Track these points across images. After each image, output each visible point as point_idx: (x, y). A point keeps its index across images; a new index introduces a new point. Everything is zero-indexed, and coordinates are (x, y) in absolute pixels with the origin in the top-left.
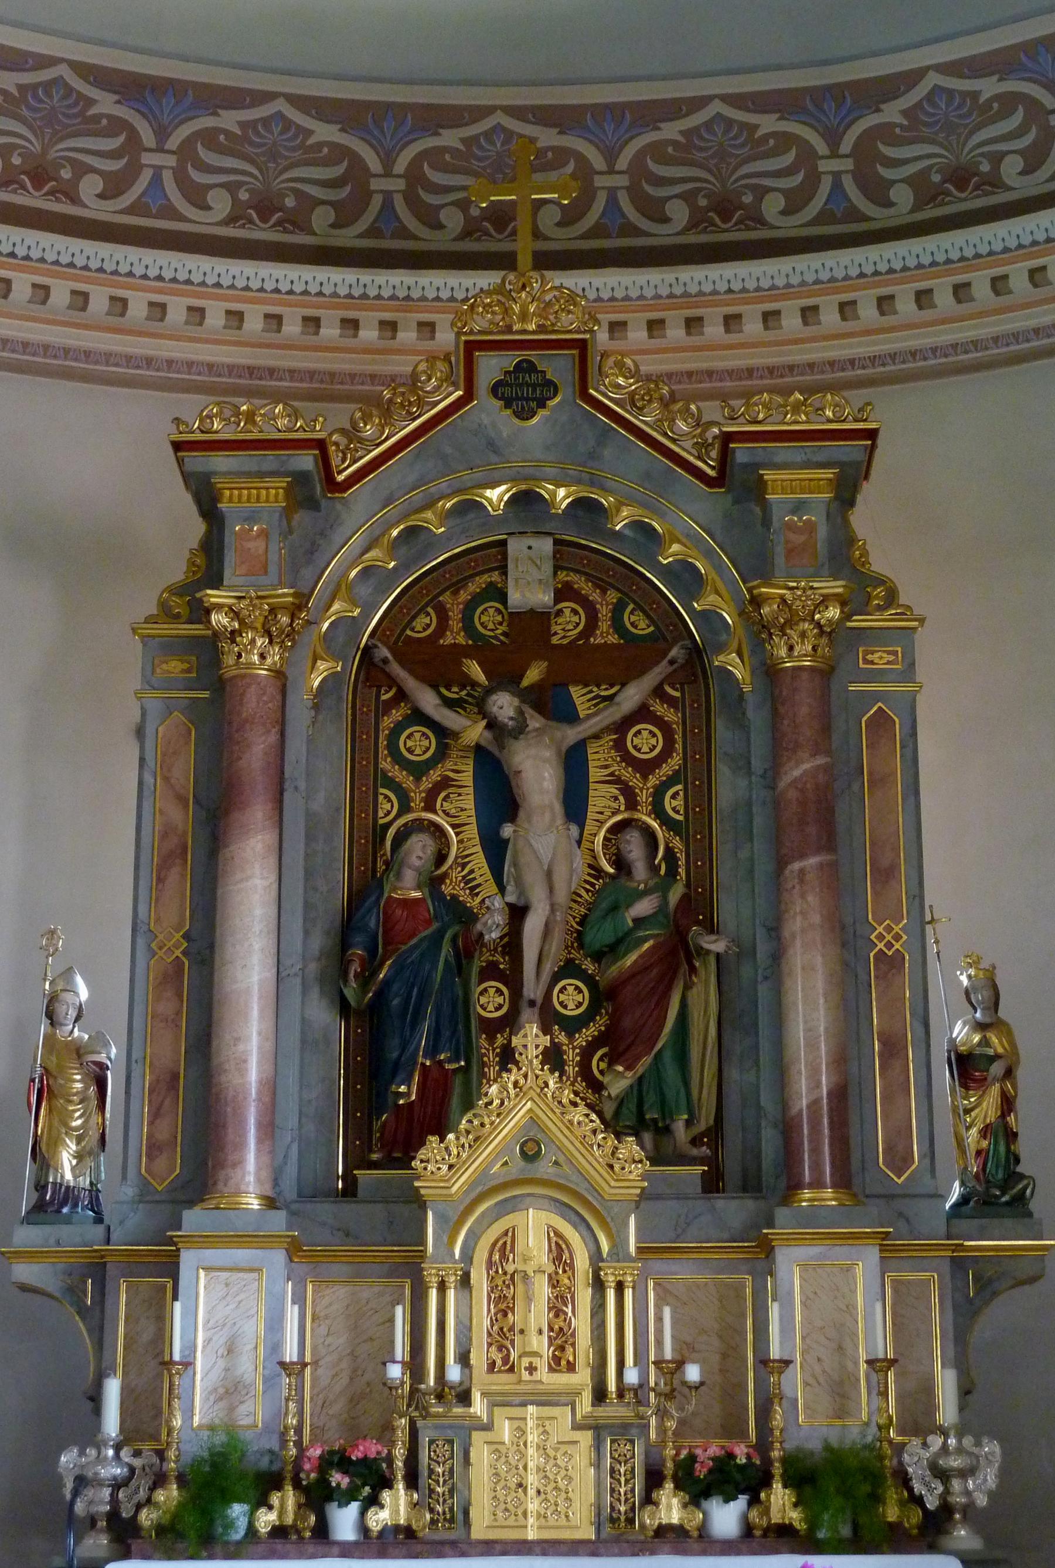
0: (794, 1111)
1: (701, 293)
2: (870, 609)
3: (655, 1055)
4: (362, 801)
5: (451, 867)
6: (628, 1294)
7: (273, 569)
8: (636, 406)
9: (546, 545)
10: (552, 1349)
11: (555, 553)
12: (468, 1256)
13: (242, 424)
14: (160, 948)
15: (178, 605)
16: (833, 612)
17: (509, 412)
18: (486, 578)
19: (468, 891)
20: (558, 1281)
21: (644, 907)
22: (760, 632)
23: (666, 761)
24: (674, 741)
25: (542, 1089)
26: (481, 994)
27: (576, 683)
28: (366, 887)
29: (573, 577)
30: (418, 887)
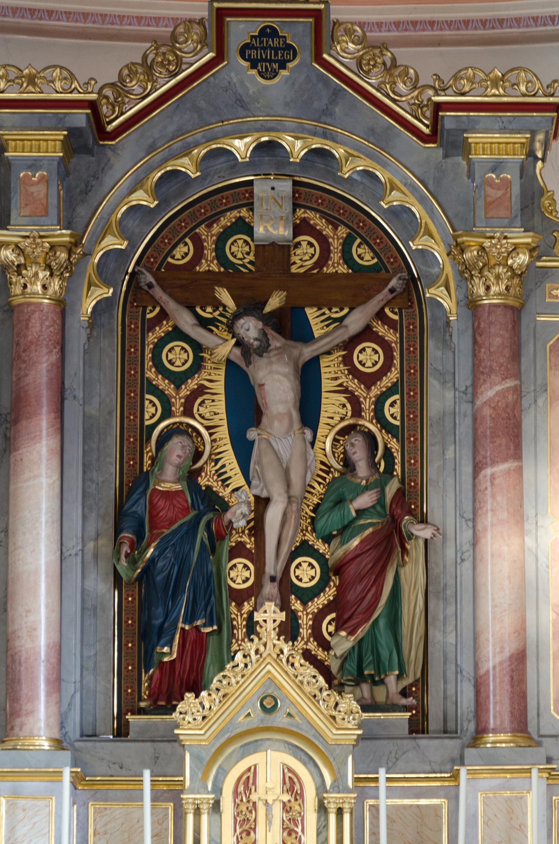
4: (130, 407)
5: (206, 463)
6: (347, 818)
7: (53, 212)
8: (362, 70)
11: (294, 192)
12: (218, 790)
17: (254, 72)
19: (220, 483)
20: (291, 808)
21: (365, 500)
23: (386, 375)
24: (392, 358)
25: (278, 655)
26: (231, 568)
27: (311, 306)
28: (134, 483)
29: (310, 214)
30: (178, 481)
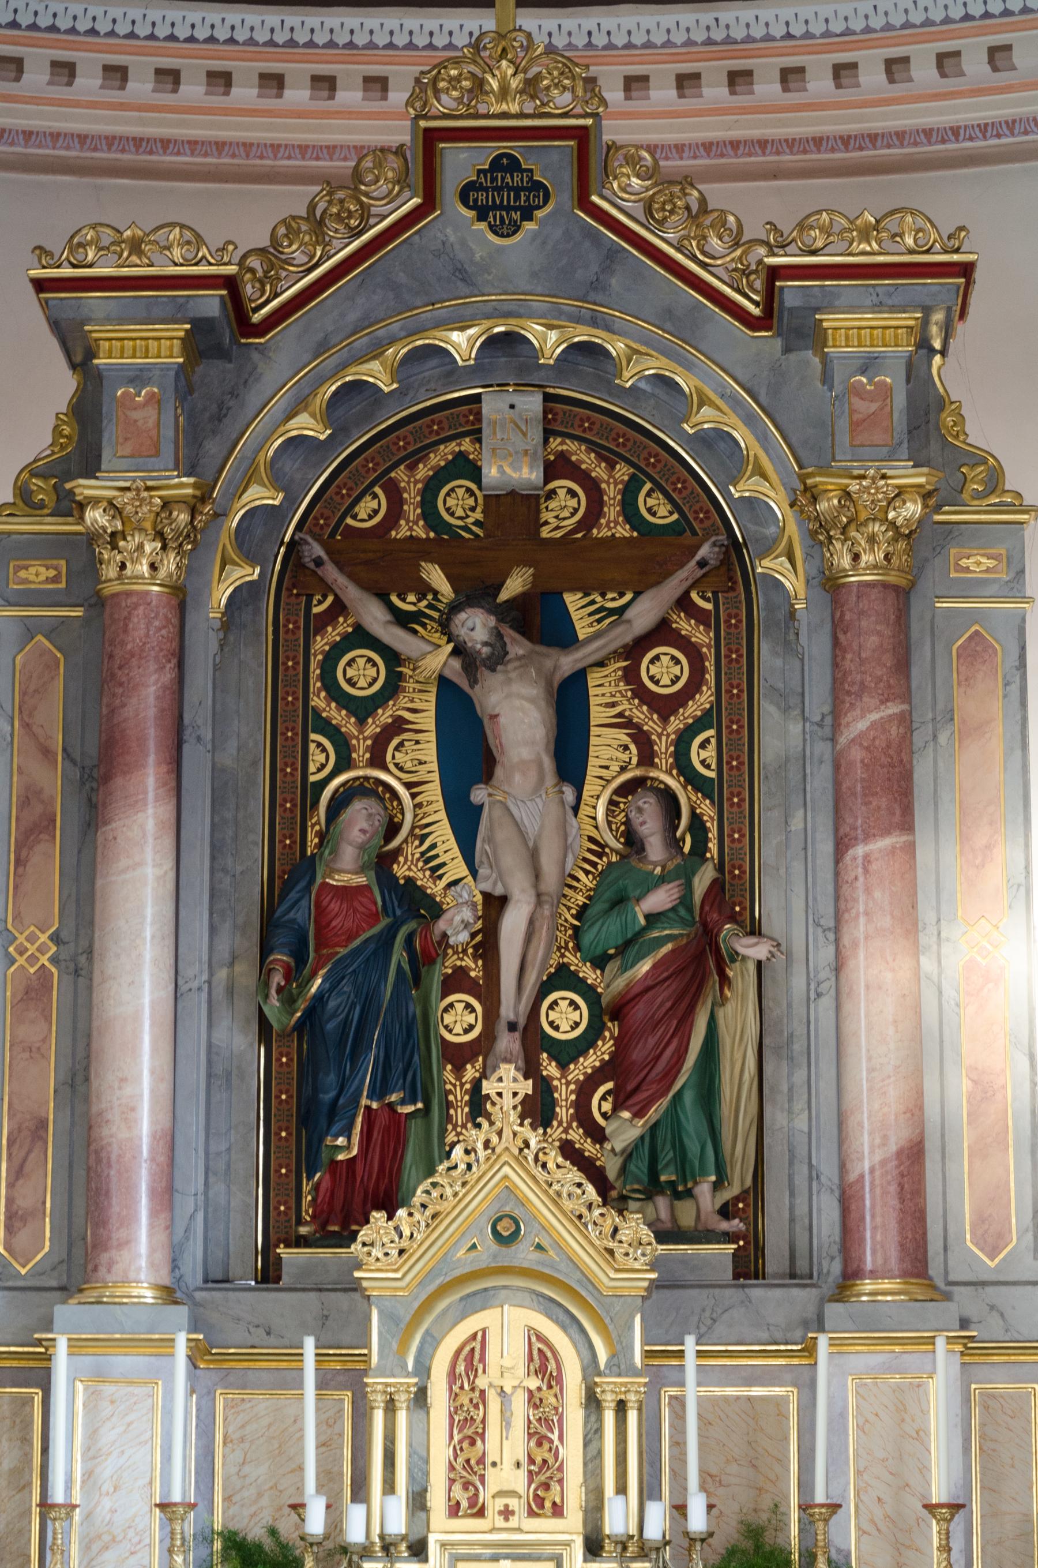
0: (852, 1177)
1: (749, 39)
2: (965, 496)
3: (674, 1097)
5: (406, 841)
6: (632, 1416)
8: (653, 218)
9: (532, 403)
10: (533, 1486)
11: (545, 413)
12: (423, 1370)
13: (125, 254)
14: (21, 954)
15: (42, 490)
16: (912, 509)
17: (483, 226)
18: (453, 446)
19: (428, 873)
20: (541, 1400)
22: (816, 532)
23: (692, 698)
24: (703, 670)
27: (573, 590)
28: (293, 873)
29: (570, 446)
30: (361, 870)
